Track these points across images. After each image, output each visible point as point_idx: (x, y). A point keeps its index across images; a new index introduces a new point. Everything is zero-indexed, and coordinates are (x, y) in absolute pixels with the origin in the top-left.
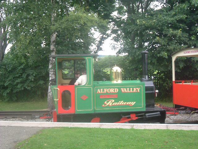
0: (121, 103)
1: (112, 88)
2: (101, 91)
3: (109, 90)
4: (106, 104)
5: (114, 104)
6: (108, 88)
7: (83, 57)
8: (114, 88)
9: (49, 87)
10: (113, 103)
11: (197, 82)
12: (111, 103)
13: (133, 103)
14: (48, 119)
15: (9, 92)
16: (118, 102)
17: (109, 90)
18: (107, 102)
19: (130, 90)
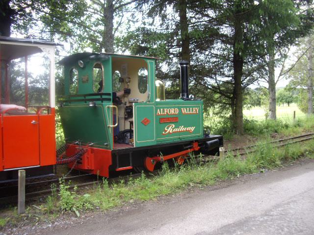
0: (182, 128)
1: (172, 107)
2: (161, 113)
3: (170, 111)
4: (166, 131)
5: (174, 131)
6: (168, 108)
7: (157, 90)
8: (174, 108)
9: (53, 104)
10: (173, 129)
11: (312, 169)
12: (172, 130)
13: (192, 129)
14: (93, 85)
15: (212, 43)
16: (178, 128)
17: (170, 111)
18: (168, 128)
19: (189, 111)
